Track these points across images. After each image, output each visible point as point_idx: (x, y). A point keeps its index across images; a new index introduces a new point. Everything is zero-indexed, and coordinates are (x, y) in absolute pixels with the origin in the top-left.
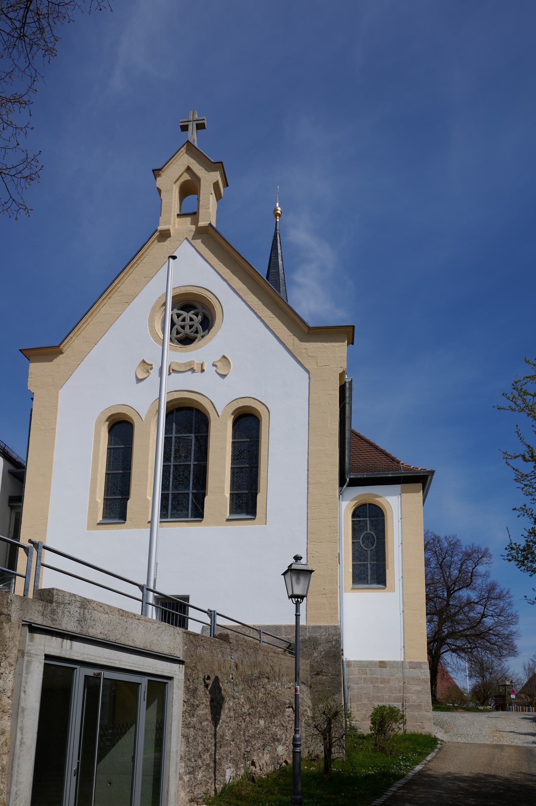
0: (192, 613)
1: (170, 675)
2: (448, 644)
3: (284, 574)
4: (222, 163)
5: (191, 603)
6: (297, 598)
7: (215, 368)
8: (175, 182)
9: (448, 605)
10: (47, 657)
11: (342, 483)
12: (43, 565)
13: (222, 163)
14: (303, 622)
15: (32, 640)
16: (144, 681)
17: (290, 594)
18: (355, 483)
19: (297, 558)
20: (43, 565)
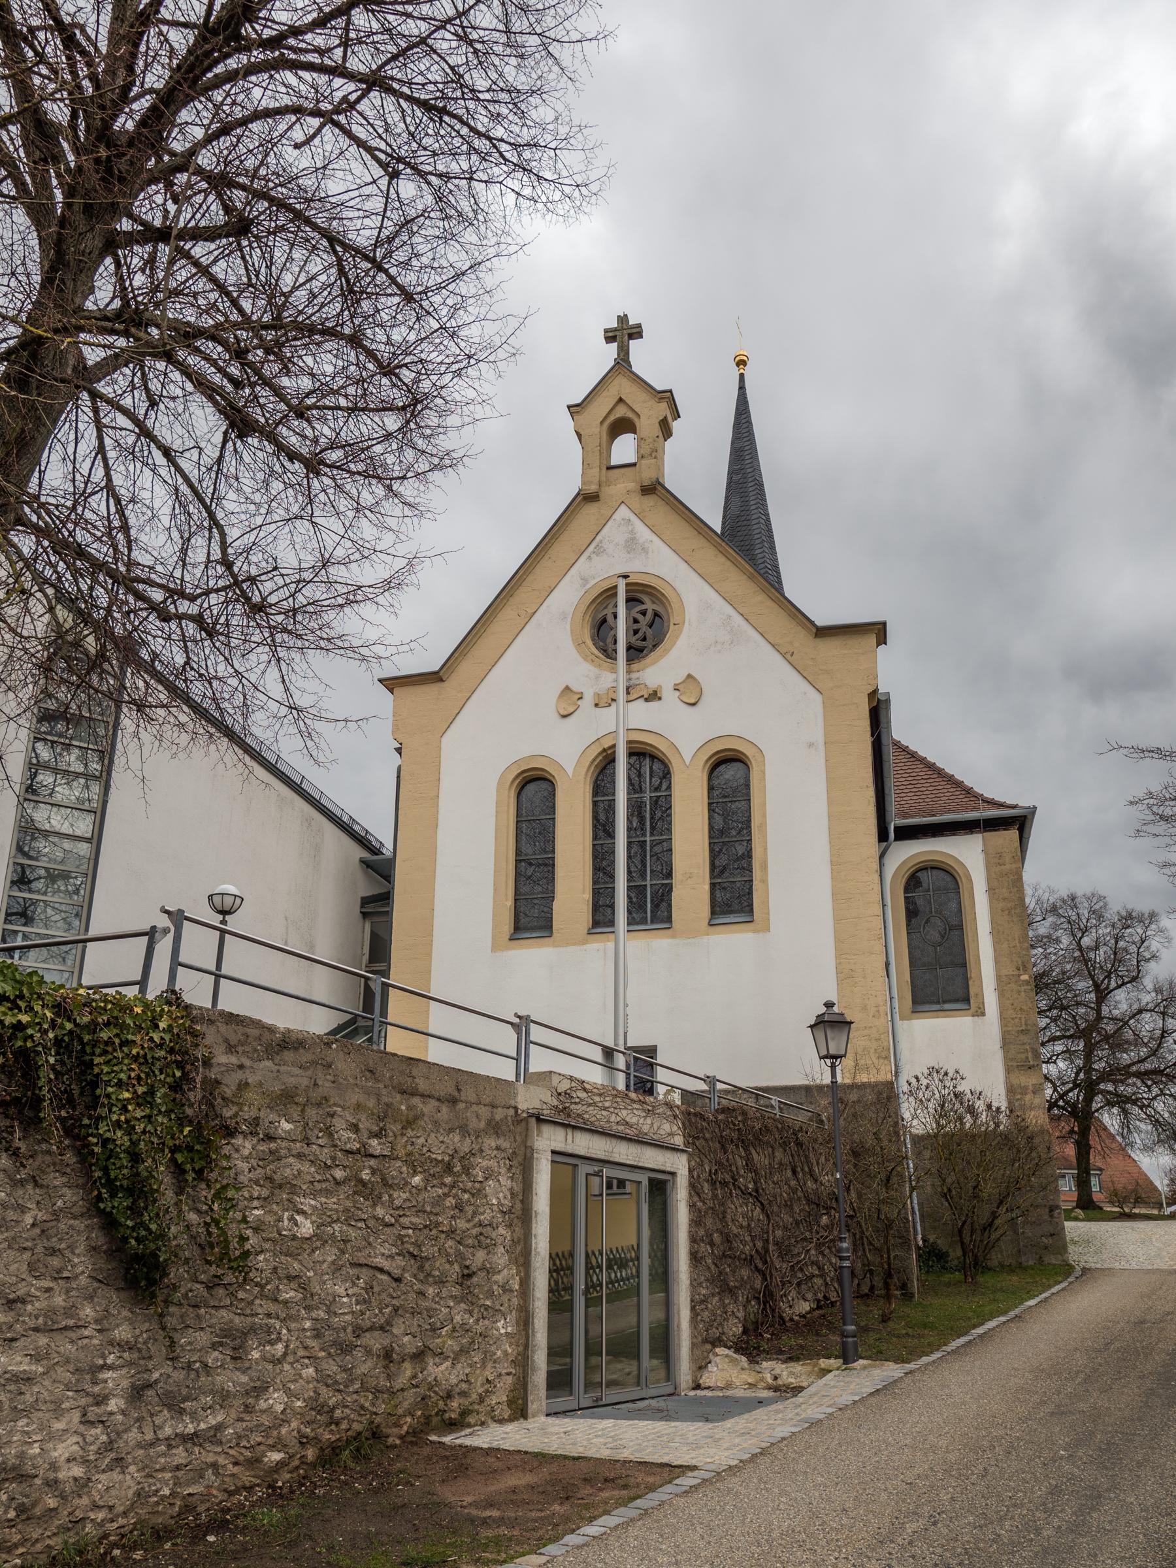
0: (661, 1075)
1: (672, 1170)
2: (1102, 1092)
3: (811, 1027)
4: (670, 391)
5: (660, 1060)
6: (834, 1058)
7: (677, 693)
8: (602, 423)
9: (1099, 1018)
10: (553, 1152)
11: (883, 836)
12: (181, 965)
13: (670, 391)
14: (839, 1079)
15: (539, 1133)
16: (644, 1178)
17: (824, 1053)
18: (907, 833)
19: (829, 1005)
20: (181, 965)
